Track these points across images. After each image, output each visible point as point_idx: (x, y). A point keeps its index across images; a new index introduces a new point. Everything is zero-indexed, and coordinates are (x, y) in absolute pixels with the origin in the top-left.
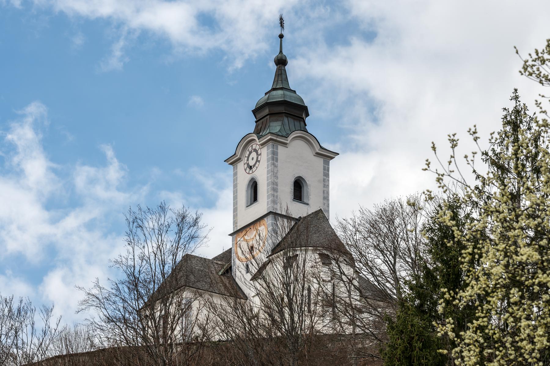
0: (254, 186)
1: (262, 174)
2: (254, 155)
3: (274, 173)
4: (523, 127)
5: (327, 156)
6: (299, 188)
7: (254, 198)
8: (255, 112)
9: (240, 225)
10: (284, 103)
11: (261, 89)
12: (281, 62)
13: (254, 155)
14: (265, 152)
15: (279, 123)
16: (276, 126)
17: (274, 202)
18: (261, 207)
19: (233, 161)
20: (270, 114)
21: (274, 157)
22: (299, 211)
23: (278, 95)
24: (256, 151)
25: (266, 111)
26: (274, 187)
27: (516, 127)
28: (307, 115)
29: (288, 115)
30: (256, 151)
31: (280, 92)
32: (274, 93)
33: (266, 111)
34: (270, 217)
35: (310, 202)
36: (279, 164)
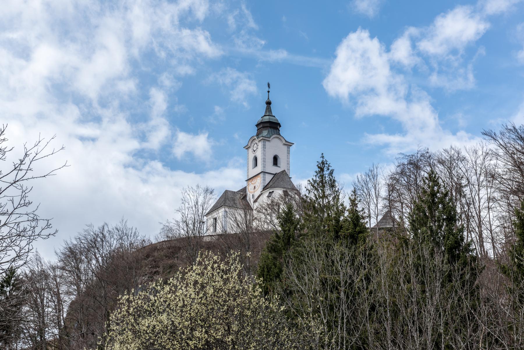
0: (256, 159)
1: (259, 154)
2: (256, 145)
3: (264, 154)
4: (325, 169)
5: (289, 145)
6: (275, 160)
7: (256, 165)
8: (257, 126)
9: (250, 177)
10: (269, 122)
11: (259, 115)
12: (269, 103)
13: (256, 145)
14: (260, 145)
15: (267, 131)
16: (265, 133)
17: (264, 167)
18: (259, 169)
19: (247, 148)
20: (263, 127)
21: (264, 147)
22: (276, 170)
23: (267, 119)
24: (256, 143)
25: (261, 126)
26: (264, 161)
27: (322, 170)
28: (280, 126)
29: (271, 127)
30: (256, 143)
31: (267, 117)
32: (265, 117)
33: (261, 126)
34: (262, 174)
35: (281, 166)
36: (266, 150)
